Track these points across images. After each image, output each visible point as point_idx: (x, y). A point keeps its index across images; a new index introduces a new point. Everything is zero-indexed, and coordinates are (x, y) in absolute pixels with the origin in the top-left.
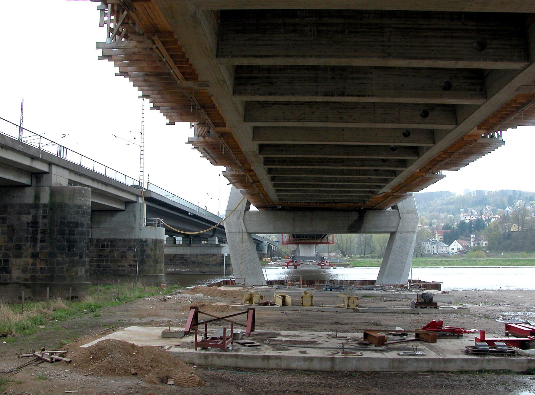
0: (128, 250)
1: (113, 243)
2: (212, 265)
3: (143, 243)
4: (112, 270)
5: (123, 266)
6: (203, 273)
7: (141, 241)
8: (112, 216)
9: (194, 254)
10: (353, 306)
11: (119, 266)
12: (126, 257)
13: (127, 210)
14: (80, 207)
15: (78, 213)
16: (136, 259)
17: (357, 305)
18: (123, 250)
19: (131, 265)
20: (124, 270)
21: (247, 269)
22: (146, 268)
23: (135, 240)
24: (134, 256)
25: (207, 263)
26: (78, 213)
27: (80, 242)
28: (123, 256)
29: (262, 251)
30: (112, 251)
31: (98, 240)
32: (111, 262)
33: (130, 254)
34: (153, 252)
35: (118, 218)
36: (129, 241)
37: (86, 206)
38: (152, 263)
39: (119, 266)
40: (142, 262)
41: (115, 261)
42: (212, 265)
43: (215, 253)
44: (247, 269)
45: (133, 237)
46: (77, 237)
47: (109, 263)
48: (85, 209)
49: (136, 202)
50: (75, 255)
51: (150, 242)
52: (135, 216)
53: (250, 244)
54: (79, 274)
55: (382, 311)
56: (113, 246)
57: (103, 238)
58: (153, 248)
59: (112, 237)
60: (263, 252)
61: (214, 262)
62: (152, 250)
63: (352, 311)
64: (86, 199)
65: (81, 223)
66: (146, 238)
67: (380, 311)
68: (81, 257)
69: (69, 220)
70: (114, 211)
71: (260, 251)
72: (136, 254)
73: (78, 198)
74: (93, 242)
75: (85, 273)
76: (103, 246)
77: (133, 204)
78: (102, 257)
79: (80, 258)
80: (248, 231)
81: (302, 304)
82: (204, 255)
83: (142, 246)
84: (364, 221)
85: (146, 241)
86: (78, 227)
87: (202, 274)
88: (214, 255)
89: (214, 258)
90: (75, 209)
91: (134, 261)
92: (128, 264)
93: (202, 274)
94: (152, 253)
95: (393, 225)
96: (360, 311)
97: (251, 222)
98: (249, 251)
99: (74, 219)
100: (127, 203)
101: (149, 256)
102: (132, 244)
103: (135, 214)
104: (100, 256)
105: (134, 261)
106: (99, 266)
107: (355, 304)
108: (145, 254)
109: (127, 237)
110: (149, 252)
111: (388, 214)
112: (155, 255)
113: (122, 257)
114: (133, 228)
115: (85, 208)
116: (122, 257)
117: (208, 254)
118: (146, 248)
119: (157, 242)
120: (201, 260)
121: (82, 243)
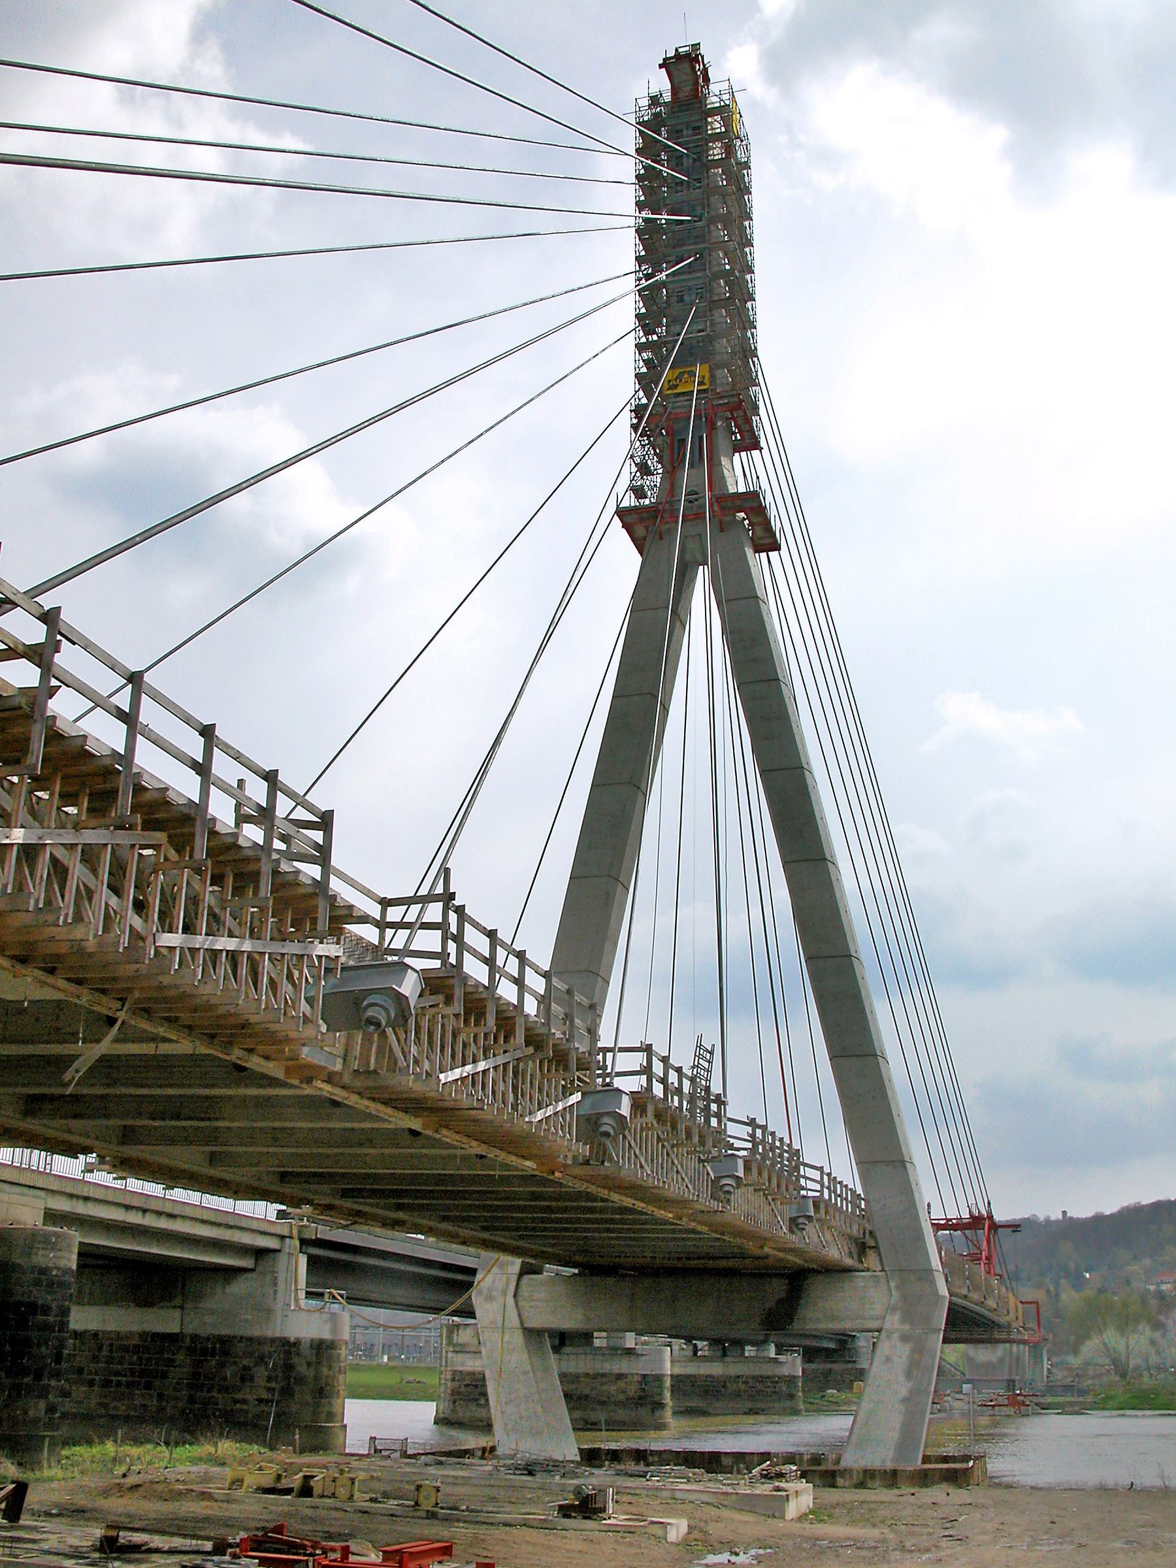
0: (256, 1364)
1: (224, 1346)
2: (616, 1403)
3: (289, 1347)
4: (219, 1410)
5: (244, 1402)
6: (592, 1424)
7: (285, 1342)
8: (227, 1281)
9: (571, 1374)
10: (427, 1505)
11: (236, 1402)
12: (252, 1379)
13: (259, 1269)
14: (43, 1271)
15: (38, 1283)
16: (273, 1385)
17: (437, 1504)
18: (245, 1362)
19: (260, 1401)
20: (247, 1412)
21: (521, 1418)
22: (294, 1408)
23: (273, 1340)
24: (269, 1379)
25: (603, 1399)
26: (38, 1283)
27: (39, 1345)
28: (246, 1377)
29: (854, 1362)
30: (222, 1365)
31: (195, 1337)
32: (219, 1391)
33: (261, 1373)
34: (312, 1369)
35: (239, 1287)
36: (261, 1341)
37: (58, 1269)
38: (308, 1398)
39: (236, 1402)
40: (287, 1392)
41: (225, 1389)
42: (616, 1403)
43: (623, 1371)
44: (521, 1418)
45: (270, 1334)
46: (34, 1335)
47: (215, 1394)
48: (56, 1276)
49: (280, 1251)
50: (25, 1372)
51: (305, 1348)
52: (275, 1284)
53: (530, 1357)
54: (31, 1413)
55: (483, 1520)
56: (225, 1353)
57: (203, 1332)
58: (314, 1359)
59: (225, 1331)
60: (858, 1367)
61: (621, 1397)
62: (309, 1364)
63: (423, 1514)
64: (58, 1254)
65: (43, 1305)
66: (297, 1336)
67: (478, 1519)
68: (38, 1376)
69: (18, 1298)
70: (231, 1273)
71: (849, 1362)
72: (273, 1374)
73: (41, 1252)
74: (183, 1342)
75: (46, 1413)
76: (204, 1352)
77: (272, 1255)
78: (199, 1379)
79: (34, 1379)
80: (525, 1326)
81: (333, 1494)
82: (595, 1377)
83: (288, 1353)
84: (802, 1302)
85: (297, 1343)
86: (35, 1314)
87: (589, 1426)
88: (620, 1377)
89: (621, 1384)
90: (32, 1276)
91: (269, 1389)
92: (255, 1397)
93: (589, 1426)
94: (310, 1373)
95: (872, 1313)
96: (440, 1516)
97: (532, 1304)
98: (525, 1373)
99: (29, 1297)
100: (261, 1253)
101: (301, 1380)
102: (267, 1348)
103: (276, 1278)
104: (196, 1375)
105: (269, 1389)
106: (192, 1400)
107: (433, 1501)
108: (293, 1375)
109: (256, 1332)
110: (302, 1368)
111: (862, 1284)
112: (316, 1378)
113: (243, 1379)
114: (269, 1311)
115: (54, 1273)
116: (243, 1379)
117: (604, 1375)
118: (295, 1360)
119: (324, 1346)
120: (587, 1391)
121: (43, 1349)
